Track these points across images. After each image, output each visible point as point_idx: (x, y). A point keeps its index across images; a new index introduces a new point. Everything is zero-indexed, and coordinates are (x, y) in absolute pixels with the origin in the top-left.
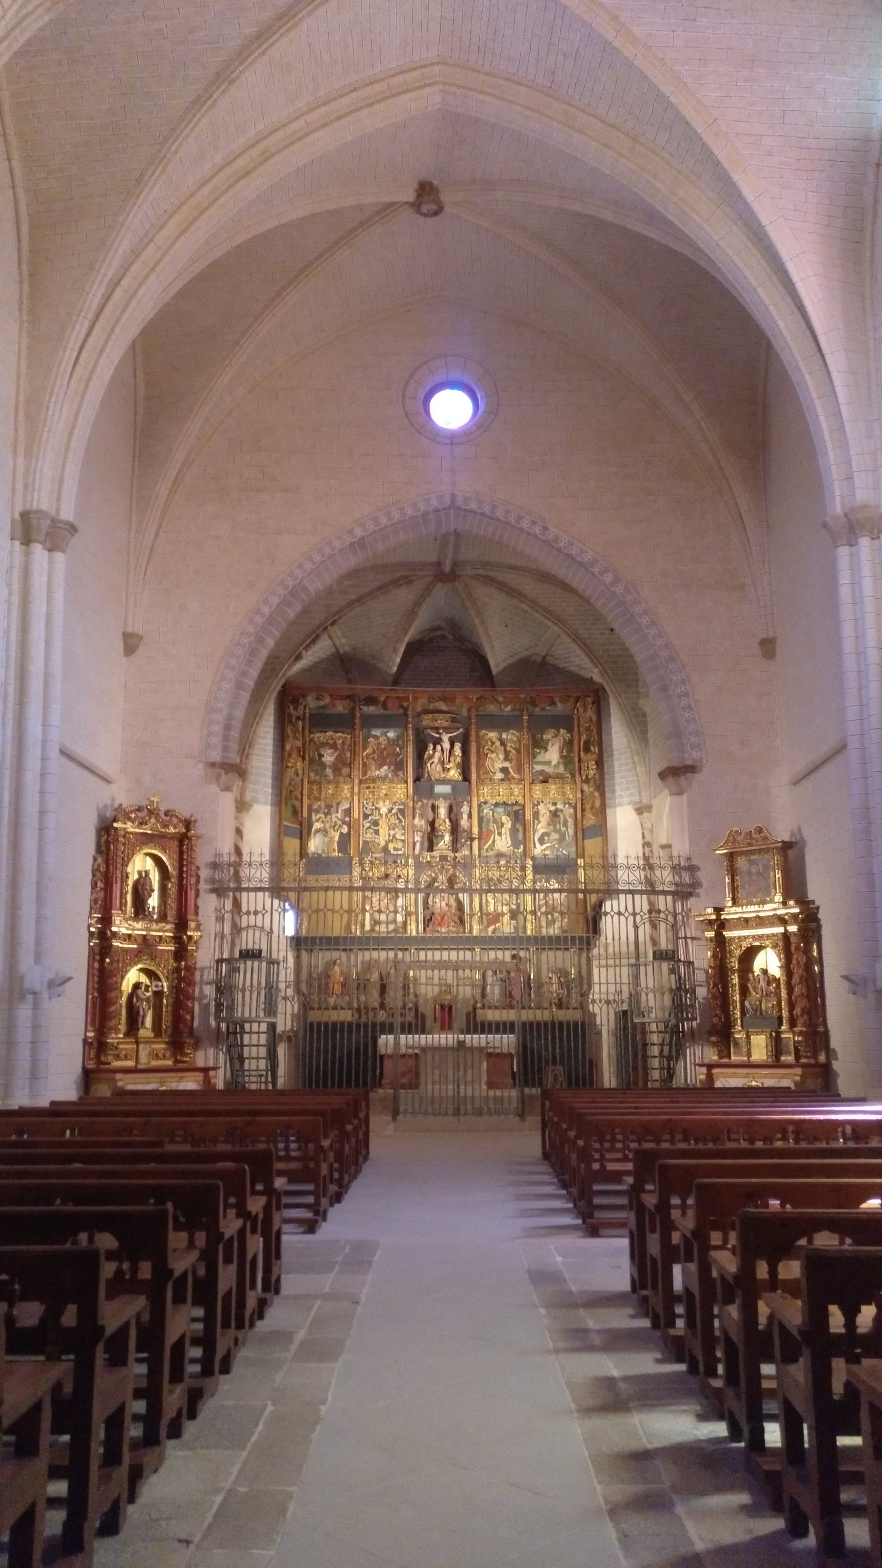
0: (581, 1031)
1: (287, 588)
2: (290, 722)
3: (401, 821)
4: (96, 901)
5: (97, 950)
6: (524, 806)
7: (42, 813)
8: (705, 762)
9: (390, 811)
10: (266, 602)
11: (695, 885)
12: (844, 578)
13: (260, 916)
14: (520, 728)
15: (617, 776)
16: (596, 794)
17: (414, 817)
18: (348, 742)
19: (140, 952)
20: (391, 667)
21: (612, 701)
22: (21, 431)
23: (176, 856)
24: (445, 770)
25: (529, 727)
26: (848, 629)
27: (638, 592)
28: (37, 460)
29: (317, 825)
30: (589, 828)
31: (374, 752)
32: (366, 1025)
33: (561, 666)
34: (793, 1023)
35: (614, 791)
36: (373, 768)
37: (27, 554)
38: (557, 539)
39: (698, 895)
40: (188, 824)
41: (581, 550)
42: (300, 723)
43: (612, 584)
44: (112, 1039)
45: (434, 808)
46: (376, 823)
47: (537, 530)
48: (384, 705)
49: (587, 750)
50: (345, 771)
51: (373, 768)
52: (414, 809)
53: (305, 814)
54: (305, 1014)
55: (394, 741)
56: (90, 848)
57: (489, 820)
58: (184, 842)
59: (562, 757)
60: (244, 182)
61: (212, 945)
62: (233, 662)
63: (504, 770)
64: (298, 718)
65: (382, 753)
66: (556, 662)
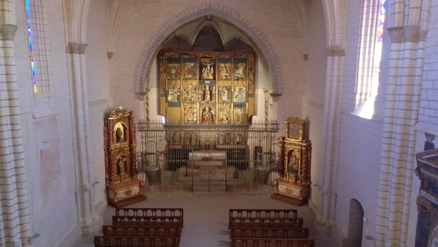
0: (244, 152)
1: (157, 36)
2: (161, 62)
4: (105, 140)
7: (86, 137)
9: (192, 88)
10: (151, 41)
11: (278, 129)
12: (329, 67)
14: (231, 63)
15: (259, 79)
21: (259, 59)
22: (65, 15)
23: (128, 123)
25: (234, 63)
26: (328, 84)
27: (267, 38)
28: (72, 24)
29: (171, 92)
32: (186, 150)
34: (301, 173)
35: (258, 84)
36: (187, 75)
37: (72, 57)
38: (243, 20)
39: (278, 132)
40: (131, 113)
41: (250, 24)
42: (164, 61)
43: (260, 35)
44: (113, 178)
45: (205, 87)
46: (188, 92)
47: (237, 16)
48: (190, 55)
49: (251, 70)
50: (178, 76)
51: (187, 75)
53: (167, 89)
54: (169, 147)
59: (243, 72)
62: (142, 61)
63: (226, 76)
64: (164, 60)
66: (243, 40)
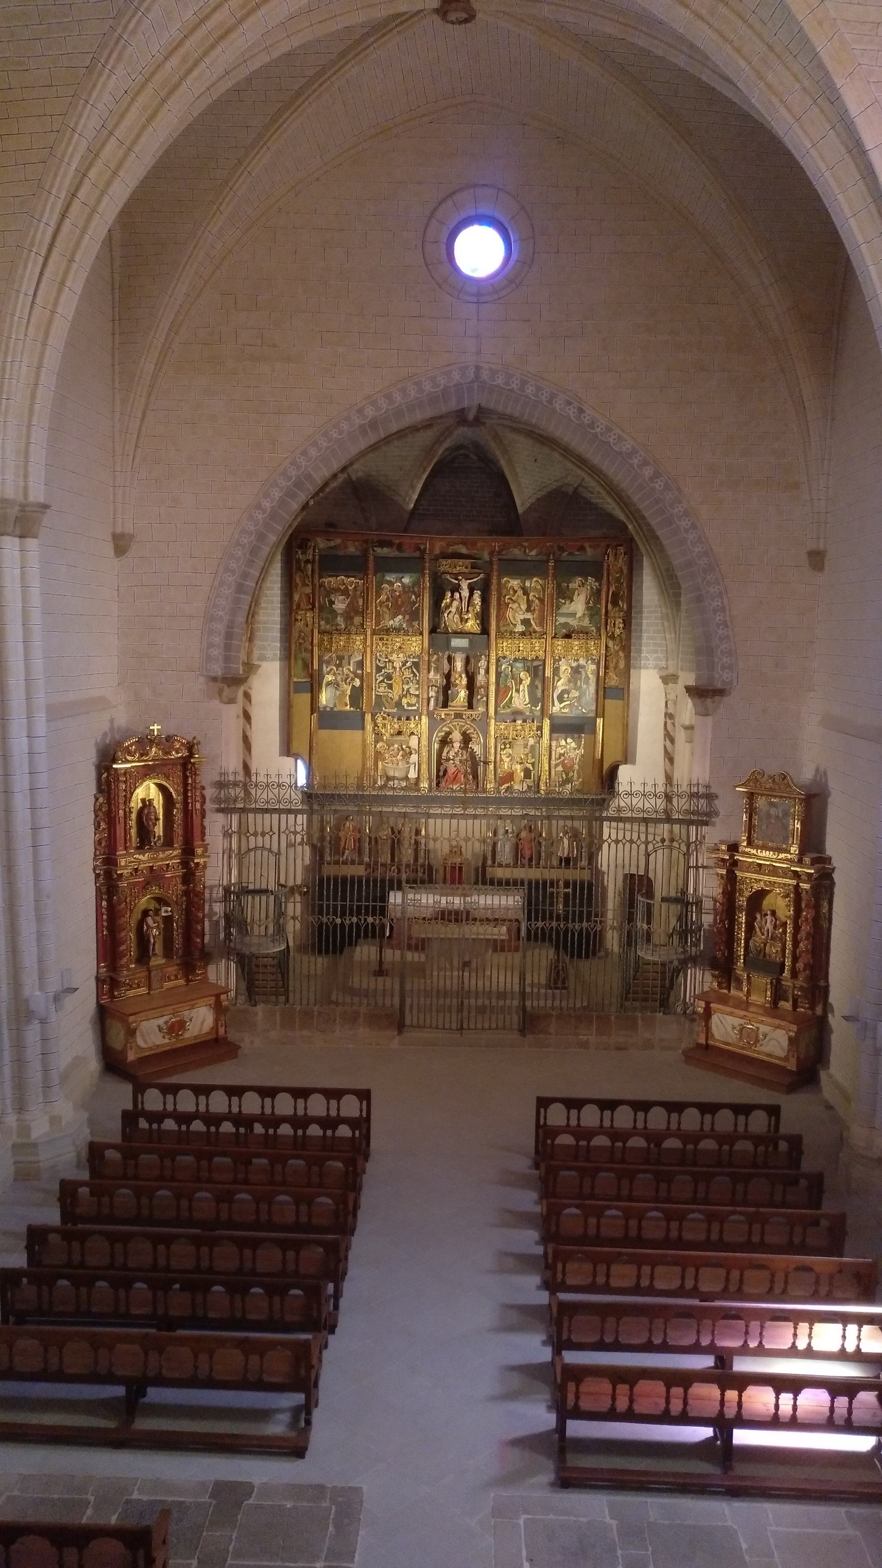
1: (290, 478)
2: (299, 569)
3: (415, 675)
4: (99, 842)
5: (104, 889)
6: (544, 661)
7: (35, 829)
8: (735, 684)
13: (267, 837)
14: (543, 574)
15: (645, 635)
16: (621, 654)
17: (429, 672)
18: (360, 588)
19: (148, 883)
20: (408, 504)
21: (646, 562)
23: (179, 781)
24: (464, 621)
27: (679, 490)
29: (329, 678)
30: (610, 688)
31: (388, 599)
33: (594, 501)
34: (794, 974)
35: (640, 652)
36: (387, 616)
40: (190, 747)
41: (620, 438)
42: (309, 566)
43: (651, 479)
44: (124, 976)
45: (450, 659)
46: (389, 677)
47: (571, 412)
48: (400, 547)
49: (615, 603)
50: (357, 620)
51: (387, 616)
52: (429, 662)
53: (316, 667)
55: (409, 587)
56: (92, 789)
57: (507, 676)
58: (187, 767)
59: (588, 608)
60: (223, 44)
61: (220, 864)
63: (526, 622)
65: (397, 601)
66: (588, 495)
